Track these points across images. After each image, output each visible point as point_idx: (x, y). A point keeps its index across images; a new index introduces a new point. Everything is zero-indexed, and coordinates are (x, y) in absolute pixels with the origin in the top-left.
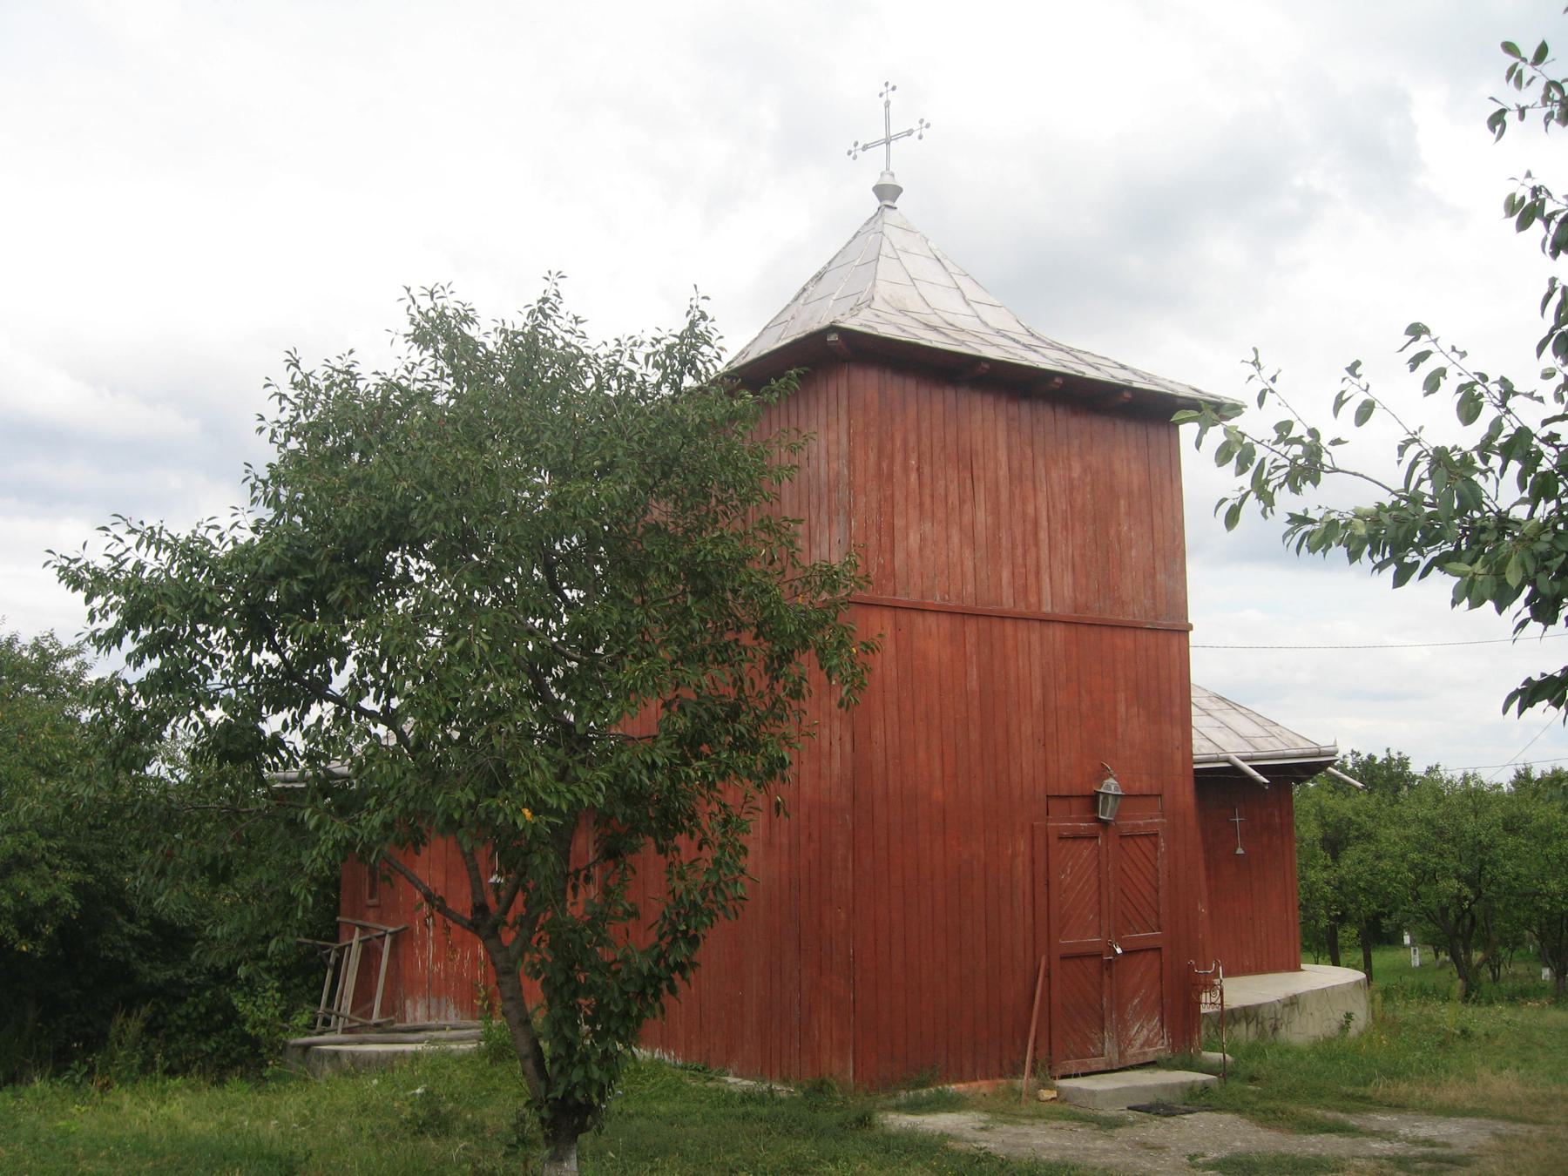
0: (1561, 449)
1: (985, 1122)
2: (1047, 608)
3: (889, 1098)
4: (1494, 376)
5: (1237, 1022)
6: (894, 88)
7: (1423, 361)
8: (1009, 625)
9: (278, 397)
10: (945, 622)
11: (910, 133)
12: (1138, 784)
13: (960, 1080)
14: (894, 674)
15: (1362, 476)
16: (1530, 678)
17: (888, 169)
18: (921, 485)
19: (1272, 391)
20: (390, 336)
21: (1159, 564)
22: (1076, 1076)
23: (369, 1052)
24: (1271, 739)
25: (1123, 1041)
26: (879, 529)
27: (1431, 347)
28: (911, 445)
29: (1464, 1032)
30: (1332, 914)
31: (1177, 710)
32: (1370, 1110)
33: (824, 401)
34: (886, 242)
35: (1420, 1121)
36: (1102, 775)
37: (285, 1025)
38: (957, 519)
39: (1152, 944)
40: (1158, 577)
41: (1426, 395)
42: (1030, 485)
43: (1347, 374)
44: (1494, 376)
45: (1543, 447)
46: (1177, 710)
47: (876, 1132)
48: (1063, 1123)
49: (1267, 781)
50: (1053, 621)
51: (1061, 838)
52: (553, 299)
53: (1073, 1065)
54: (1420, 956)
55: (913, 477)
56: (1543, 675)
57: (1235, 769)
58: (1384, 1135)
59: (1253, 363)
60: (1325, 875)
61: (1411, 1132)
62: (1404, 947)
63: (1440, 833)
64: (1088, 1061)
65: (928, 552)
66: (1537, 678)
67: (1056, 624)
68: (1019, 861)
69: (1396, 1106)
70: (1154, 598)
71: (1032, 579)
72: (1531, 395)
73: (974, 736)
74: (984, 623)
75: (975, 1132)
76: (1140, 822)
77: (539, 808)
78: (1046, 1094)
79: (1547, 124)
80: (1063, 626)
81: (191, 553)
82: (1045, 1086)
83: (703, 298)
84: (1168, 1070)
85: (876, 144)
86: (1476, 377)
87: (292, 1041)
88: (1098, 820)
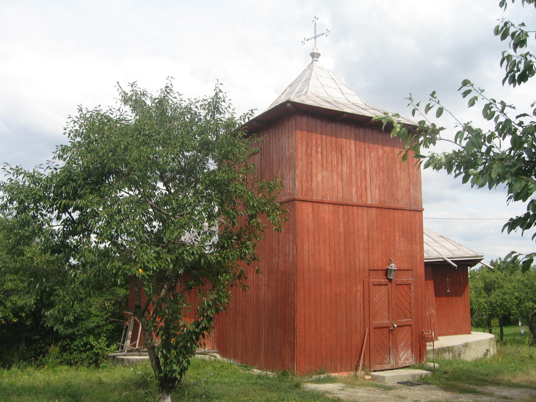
0: (524, 127)
1: (343, 387)
2: (369, 202)
3: (309, 378)
4: (498, 101)
5: (445, 352)
6: (318, 19)
7: (468, 94)
8: (355, 208)
9: (73, 122)
10: (331, 207)
11: (323, 34)
12: (403, 266)
13: (336, 371)
14: (312, 226)
15: (450, 141)
16: (512, 218)
17: (315, 47)
18: (322, 158)
19: (417, 110)
20: (116, 100)
21: (412, 187)
22: (378, 371)
23: (134, 359)
24: (459, 251)
25: (396, 358)
26: (307, 174)
27: (471, 88)
28: (319, 143)
29: (531, 356)
30: (487, 313)
31: (418, 239)
32: (487, 385)
33: (287, 127)
34: (313, 73)
35: (504, 389)
36: (390, 262)
37: (108, 349)
38: (336, 170)
39: (408, 324)
40: (411, 191)
41: (470, 107)
42: (363, 158)
43: (431, 97)
44: (498, 101)
45: (517, 127)
46: (418, 239)
47: (301, 390)
48: (371, 388)
49: (456, 266)
50: (371, 207)
51: (374, 285)
52: (170, 86)
53: (378, 367)
54: (524, 330)
55: (320, 155)
56: (517, 217)
57: (445, 261)
58: (489, 395)
59: (409, 99)
60: (485, 300)
61: (500, 393)
62: (519, 326)
63: (526, 285)
64: (384, 366)
65: (325, 182)
66: (514, 218)
67: (373, 208)
68: (358, 293)
69: (497, 384)
70: (410, 198)
71: (364, 192)
72: (510, 106)
73: (342, 248)
74: (346, 207)
75: (338, 391)
76: (404, 280)
77: (145, 269)
78: (367, 377)
79: (523, 3)
80: (375, 208)
81: (34, 178)
82: (367, 374)
83: (221, 84)
84: (414, 369)
85: (311, 39)
86: (492, 101)
87: (109, 355)
88: (388, 279)
